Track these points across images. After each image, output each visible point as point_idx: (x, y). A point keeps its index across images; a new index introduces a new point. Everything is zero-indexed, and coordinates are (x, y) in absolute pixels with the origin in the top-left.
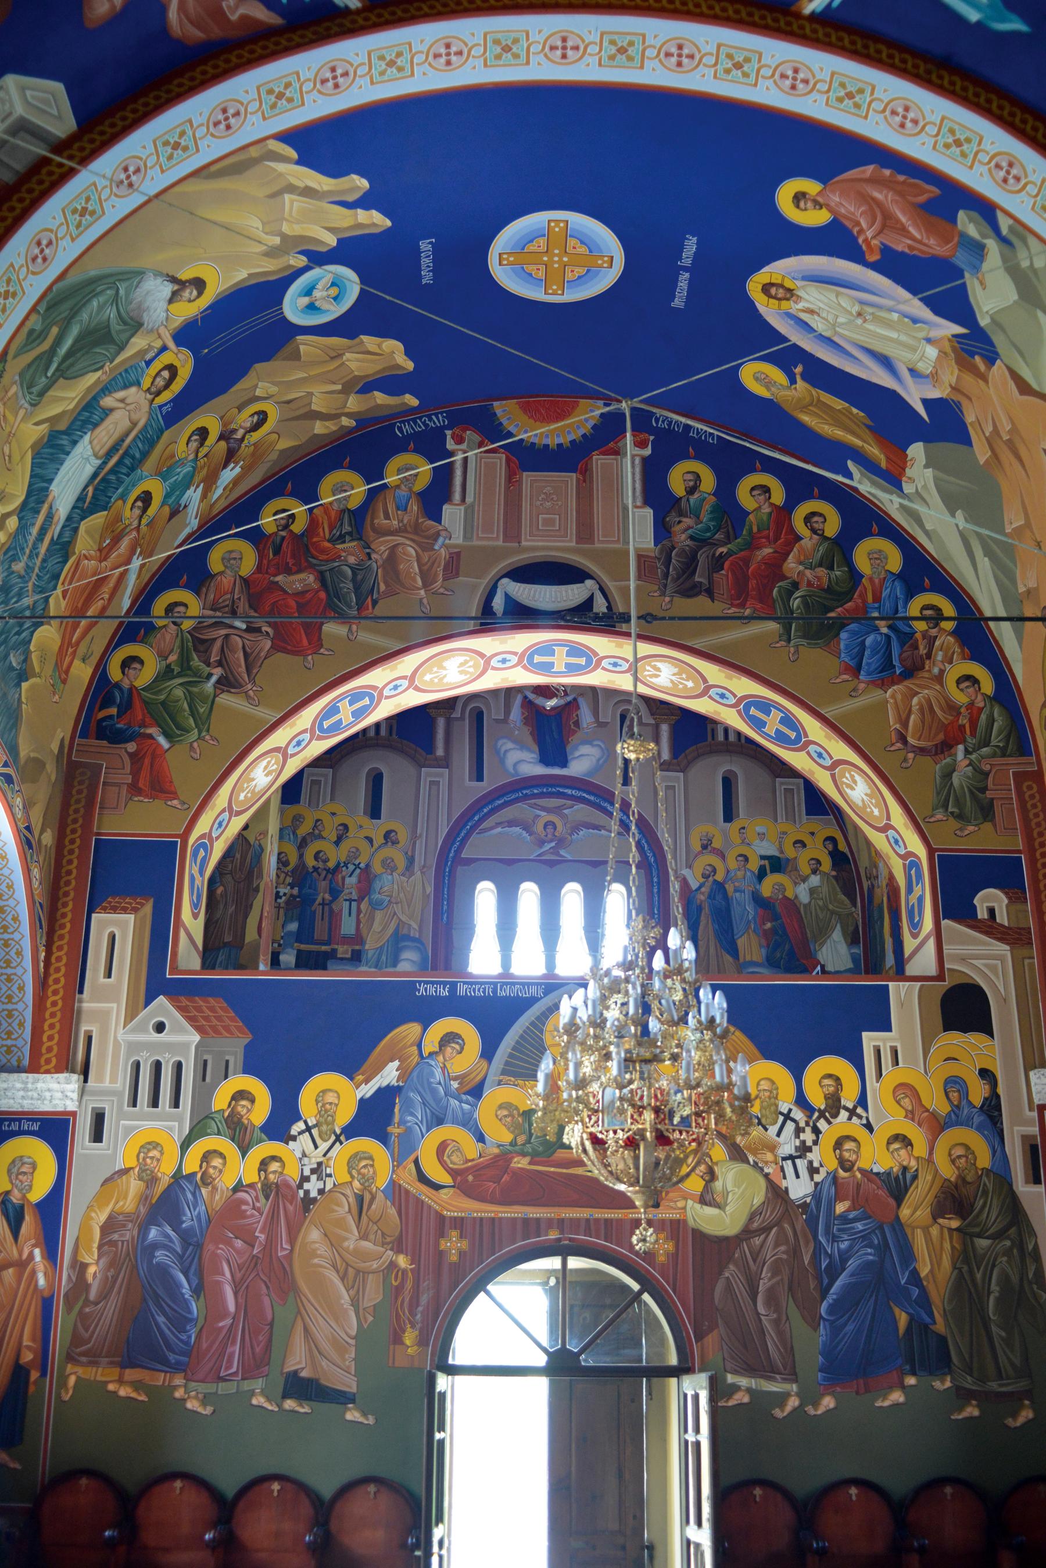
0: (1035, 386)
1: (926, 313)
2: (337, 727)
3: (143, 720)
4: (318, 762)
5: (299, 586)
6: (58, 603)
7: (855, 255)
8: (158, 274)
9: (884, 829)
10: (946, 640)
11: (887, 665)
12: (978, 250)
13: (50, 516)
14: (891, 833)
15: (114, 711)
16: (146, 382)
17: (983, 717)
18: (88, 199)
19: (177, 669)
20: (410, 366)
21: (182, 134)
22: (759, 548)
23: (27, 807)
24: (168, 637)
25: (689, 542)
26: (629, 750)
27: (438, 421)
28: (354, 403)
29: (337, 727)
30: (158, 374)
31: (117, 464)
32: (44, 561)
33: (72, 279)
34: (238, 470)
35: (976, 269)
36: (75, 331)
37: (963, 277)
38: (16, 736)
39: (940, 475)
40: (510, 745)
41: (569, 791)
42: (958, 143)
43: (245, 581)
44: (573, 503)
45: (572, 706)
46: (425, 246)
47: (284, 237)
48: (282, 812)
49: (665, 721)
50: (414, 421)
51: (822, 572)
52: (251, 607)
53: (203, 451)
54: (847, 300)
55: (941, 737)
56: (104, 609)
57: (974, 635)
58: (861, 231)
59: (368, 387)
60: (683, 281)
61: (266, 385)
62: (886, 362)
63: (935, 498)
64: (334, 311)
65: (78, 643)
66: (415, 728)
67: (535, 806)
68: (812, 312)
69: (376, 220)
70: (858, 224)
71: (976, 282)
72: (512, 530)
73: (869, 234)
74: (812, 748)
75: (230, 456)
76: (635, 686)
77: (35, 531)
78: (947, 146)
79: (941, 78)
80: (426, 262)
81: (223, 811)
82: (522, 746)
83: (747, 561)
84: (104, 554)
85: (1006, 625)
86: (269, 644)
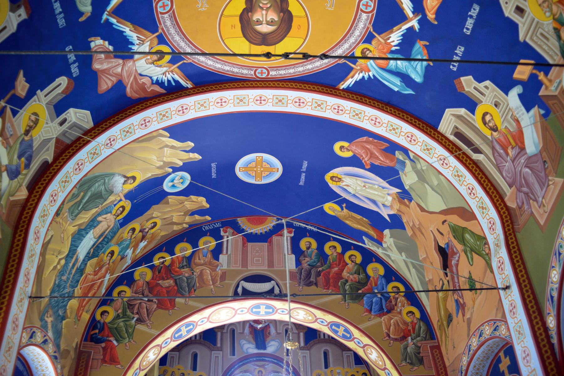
0: (426, 209)
1: (387, 185)
2: (180, 336)
3: (108, 335)
4: (173, 350)
5: (167, 285)
6: (78, 291)
7: (362, 166)
8: (119, 175)
9: (384, 369)
10: (401, 299)
11: (381, 309)
12: (403, 164)
13: (77, 260)
14: (386, 371)
15: (97, 331)
16: (114, 212)
17: (417, 326)
18: (96, 149)
19: (121, 316)
20: (208, 206)
21: (130, 128)
22: (333, 268)
23: (62, 368)
24: (118, 304)
25: (308, 267)
26: (288, 346)
27: (218, 225)
28: (188, 219)
29: (180, 336)
30: (118, 209)
31: (102, 241)
32: (74, 276)
33: (89, 176)
34: (146, 243)
35: (403, 170)
36: (89, 194)
37: (399, 174)
38: (59, 342)
39: (395, 240)
40: (245, 342)
41: (267, 359)
42: (394, 129)
43: (148, 283)
44: (266, 254)
45: (267, 327)
46: (213, 165)
47: (164, 162)
48: (159, 369)
49: (301, 332)
50: (209, 225)
51: (356, 276)
52: (149, 292)
53: (134, 236)
54: (359, 181)
55: (402, 334)
56: (95, 293)
57: (412, 297)
58: (363, 158)
59: (193, 214)
60: (303, 176)
61: (156, 213)
62: (374, 202)
63: (394, 248)
64: (181, 187)
65: (85, 306)
66: (209, 336)
67: (255, 365)
68: (348, 186)
69: (197, 157)
70: (362, 156)
71: (404, 175)
72: (245, 263)
73: (366, 159)
74: (355, 340)
75: (143, 238)
76: (290, 319)
77: (71, 265)
78: (390, 130)
79: (387, 108)
80: (214, 171)
81: (137, 369)
82: (250, 342)
83: (329, 273)
84: (96, 273)
85: (423, 294)
86: (156, 306)
